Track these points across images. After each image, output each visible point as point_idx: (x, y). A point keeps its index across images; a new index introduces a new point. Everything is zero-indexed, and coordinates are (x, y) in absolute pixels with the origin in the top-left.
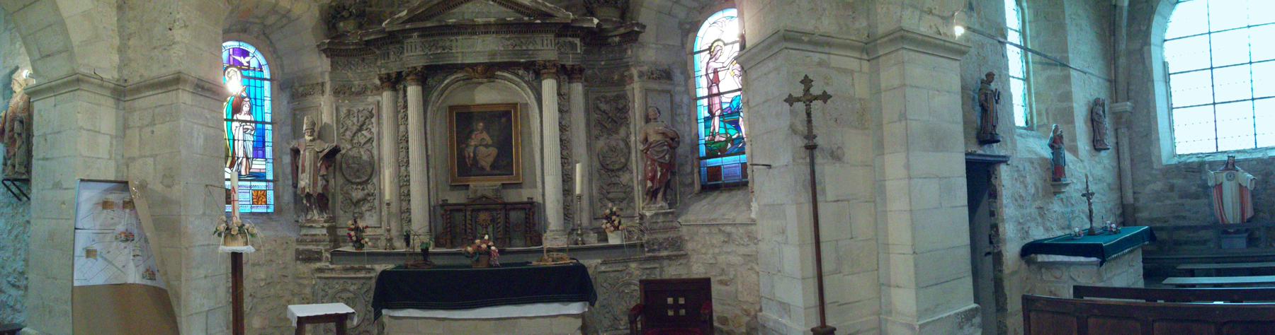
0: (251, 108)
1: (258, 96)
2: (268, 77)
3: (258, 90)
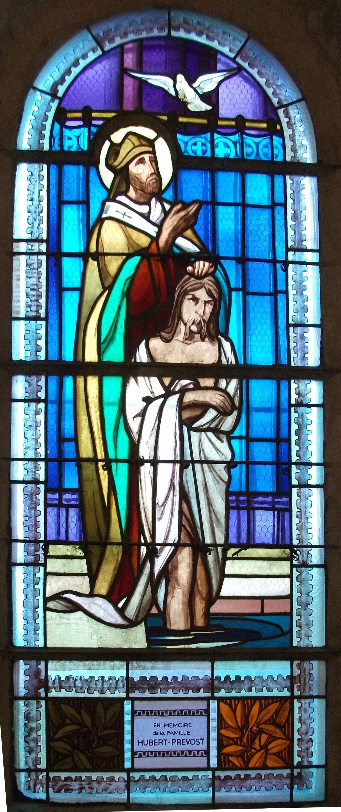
0: (220, 303)
1: (259, 247)
2: (307, 156)
3: (259, 221)
